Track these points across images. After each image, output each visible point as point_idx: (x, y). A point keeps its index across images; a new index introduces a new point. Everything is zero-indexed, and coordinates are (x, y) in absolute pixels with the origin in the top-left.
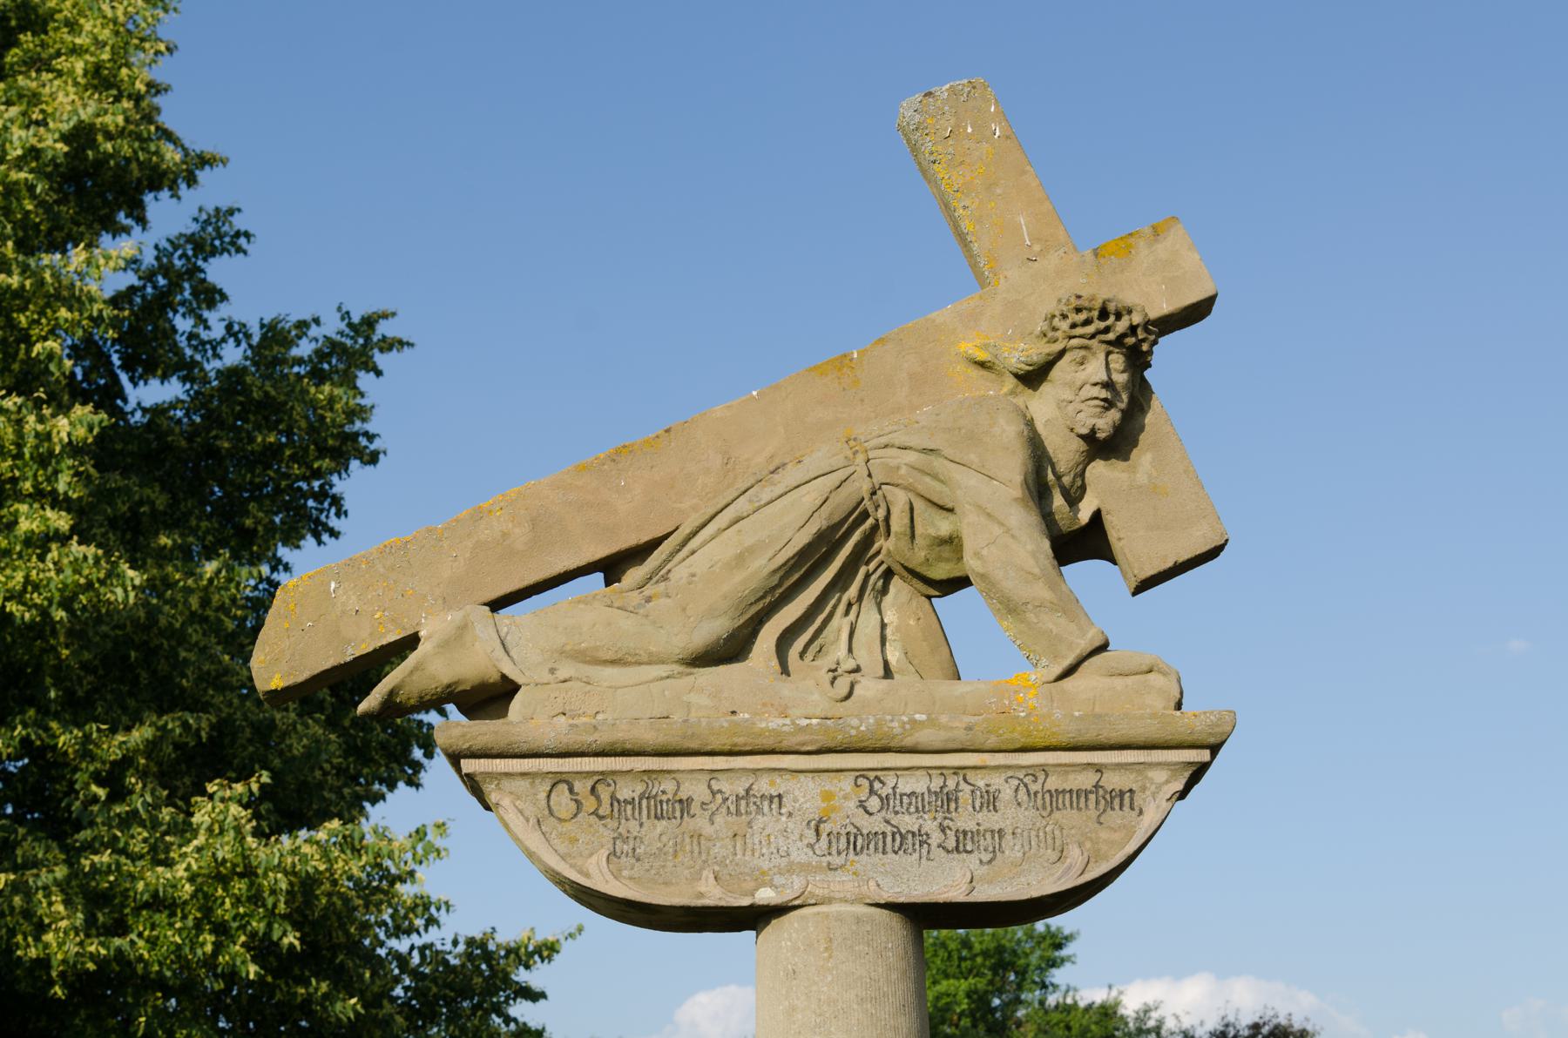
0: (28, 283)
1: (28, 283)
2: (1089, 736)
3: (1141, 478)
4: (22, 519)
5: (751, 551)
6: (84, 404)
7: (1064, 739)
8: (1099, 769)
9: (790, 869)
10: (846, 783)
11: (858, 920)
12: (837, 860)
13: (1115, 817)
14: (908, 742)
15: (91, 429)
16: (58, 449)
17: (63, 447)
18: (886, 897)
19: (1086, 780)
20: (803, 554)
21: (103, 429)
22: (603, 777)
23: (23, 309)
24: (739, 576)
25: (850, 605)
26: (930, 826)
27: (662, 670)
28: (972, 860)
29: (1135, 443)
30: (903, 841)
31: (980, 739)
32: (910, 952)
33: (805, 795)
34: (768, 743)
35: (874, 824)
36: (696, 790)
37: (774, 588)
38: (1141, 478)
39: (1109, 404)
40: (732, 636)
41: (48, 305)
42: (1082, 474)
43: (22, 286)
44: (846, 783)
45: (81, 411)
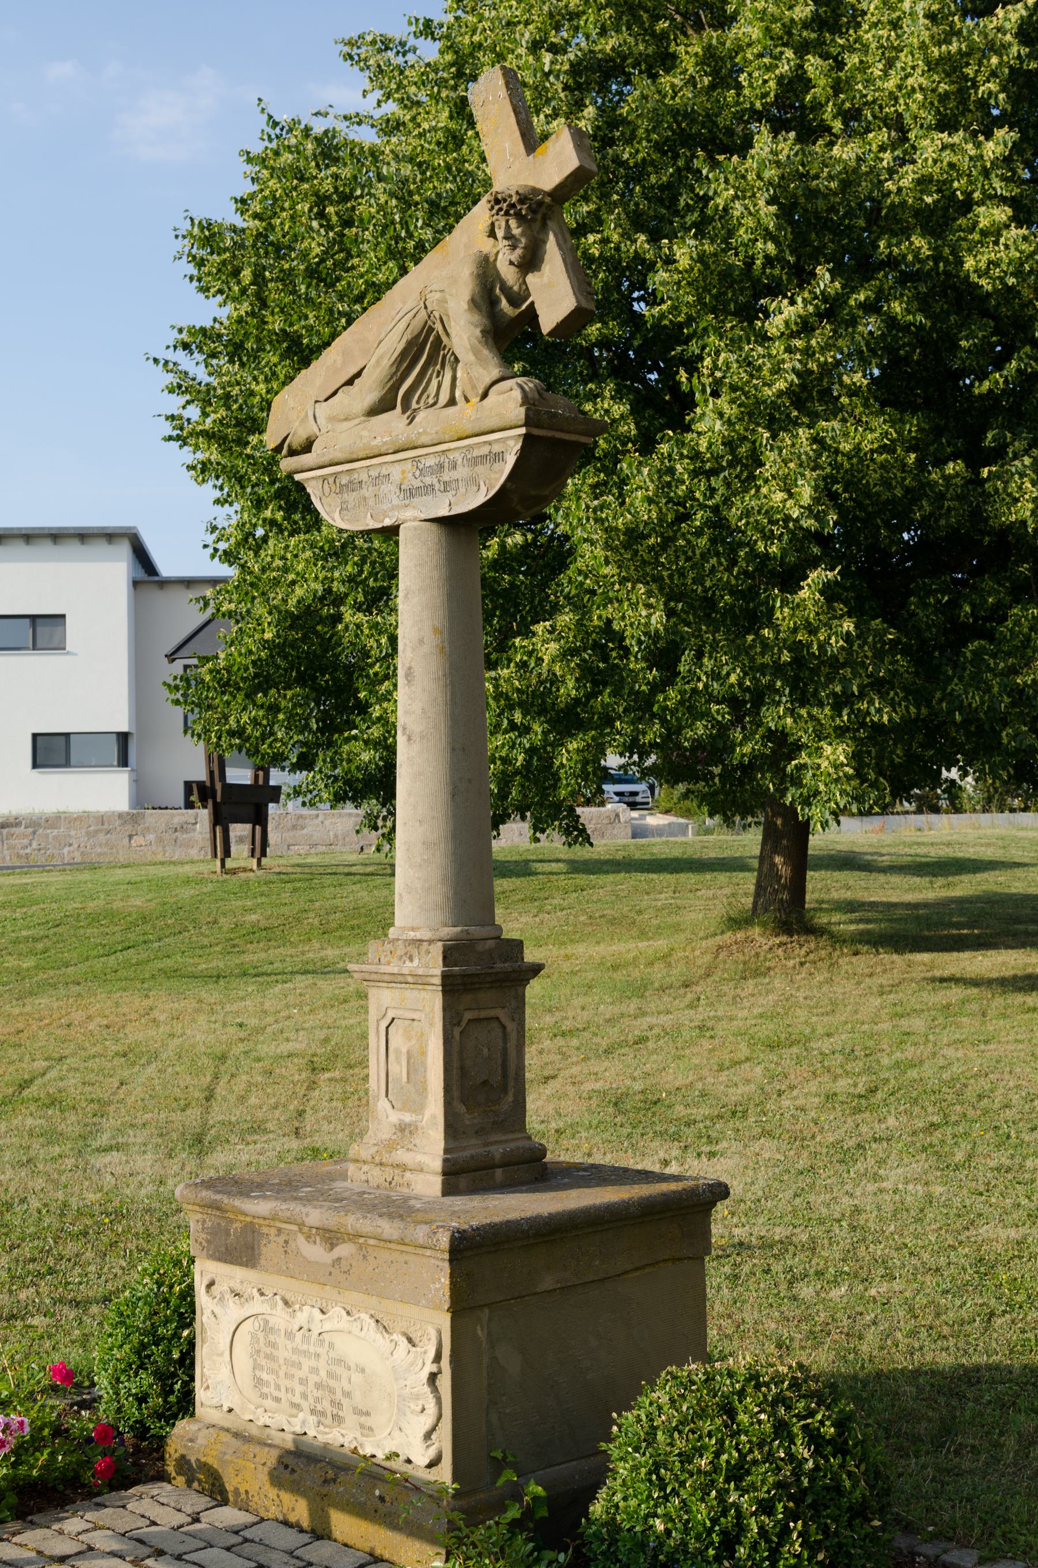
0: (963, 46)
1: (963, 46)
2: (476, 430)
3: (545, 280)
4: (981, 219)
5: (381, 357)
6: (1002, 127)
7: (469, 432)
8: (490, 443)
9: (393, 509)
10: (408, 465)
11: (415, 529)
12: (407, 502)
13: (497, 466)
14: (419, 443)
15: (1006, 146)
16: (988, 165)
17: (992, 163)
18: (423, 516)
19: (485, 450)
20: (403, 354)
21: (1014, 143)
22: (336, 475)
23: (968, 64)
24: (378, 370)
25: (439, 372)
26: (435, 481)
27: (357, 421)
28: (450, 494)
29: (542, 261)
30: (429, 489)
31: (442, 438)
32: (443, 539)
33: (396, 472)
34: (376, 452)
35: (417, 483)
36: (364, 477)
37: (395, 373)
38: (545, 280)
39: (513, 247)
40: (382, 400)
41: (984, 56)
42: (524, 282)
43: (960, 49)
44: (408, 465)
45: (1000, 133)
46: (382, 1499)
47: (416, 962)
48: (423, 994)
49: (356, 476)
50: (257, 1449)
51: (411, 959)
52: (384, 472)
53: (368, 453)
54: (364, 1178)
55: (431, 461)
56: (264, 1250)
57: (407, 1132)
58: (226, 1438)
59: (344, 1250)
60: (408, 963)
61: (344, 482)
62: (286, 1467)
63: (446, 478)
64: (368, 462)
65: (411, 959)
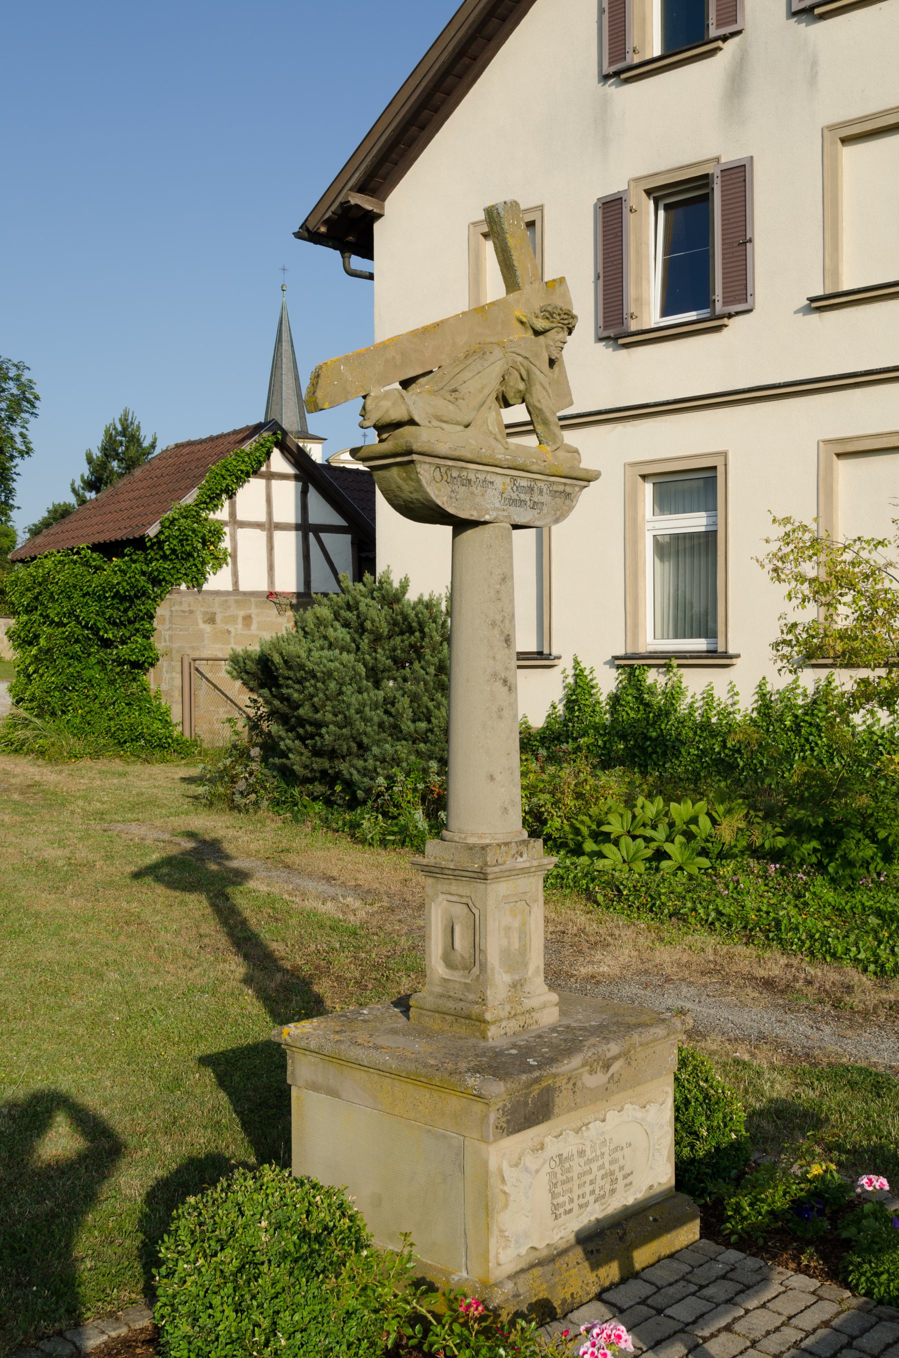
10: (508, 480)
28: (535, 512)
30: (521, 503)
33: (498, 480)
34: (496, 463)
36: (472, 476)
44: (508, 480)
46: (655, 1220)
47: (525, 856)
48: (531, 879)
49: (465, 473)
50: (566, 1258)
51: (521, 855)
52: (489, 478)
53: (491, 461)
54: (503, 1032)
55: (524, 483)
56: (557, 1100)
57: (519, 987)
58: (537, 1271)
59: (615, 1067)
60: (520, 859)
61: (454, 475)
62: (592, 1252)
63: (535, 499)
64: (450, 463)
65: (521, 855)
